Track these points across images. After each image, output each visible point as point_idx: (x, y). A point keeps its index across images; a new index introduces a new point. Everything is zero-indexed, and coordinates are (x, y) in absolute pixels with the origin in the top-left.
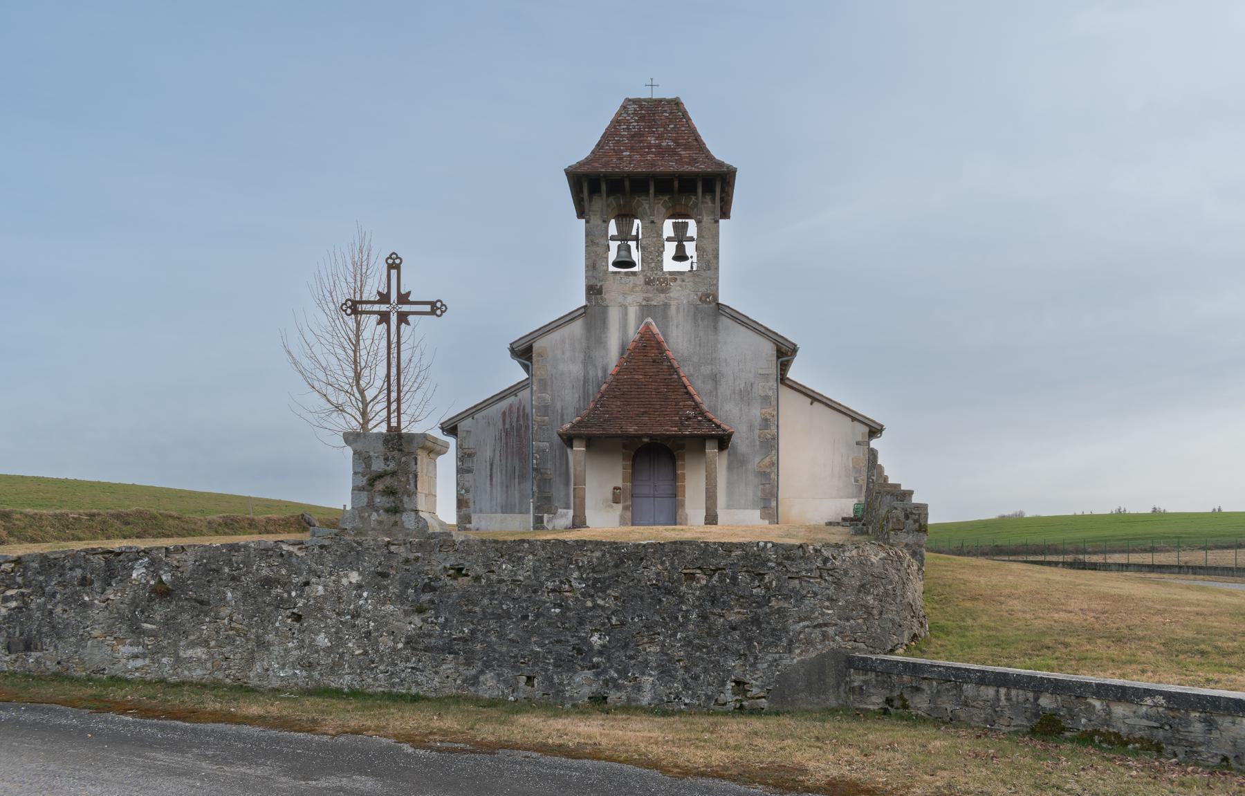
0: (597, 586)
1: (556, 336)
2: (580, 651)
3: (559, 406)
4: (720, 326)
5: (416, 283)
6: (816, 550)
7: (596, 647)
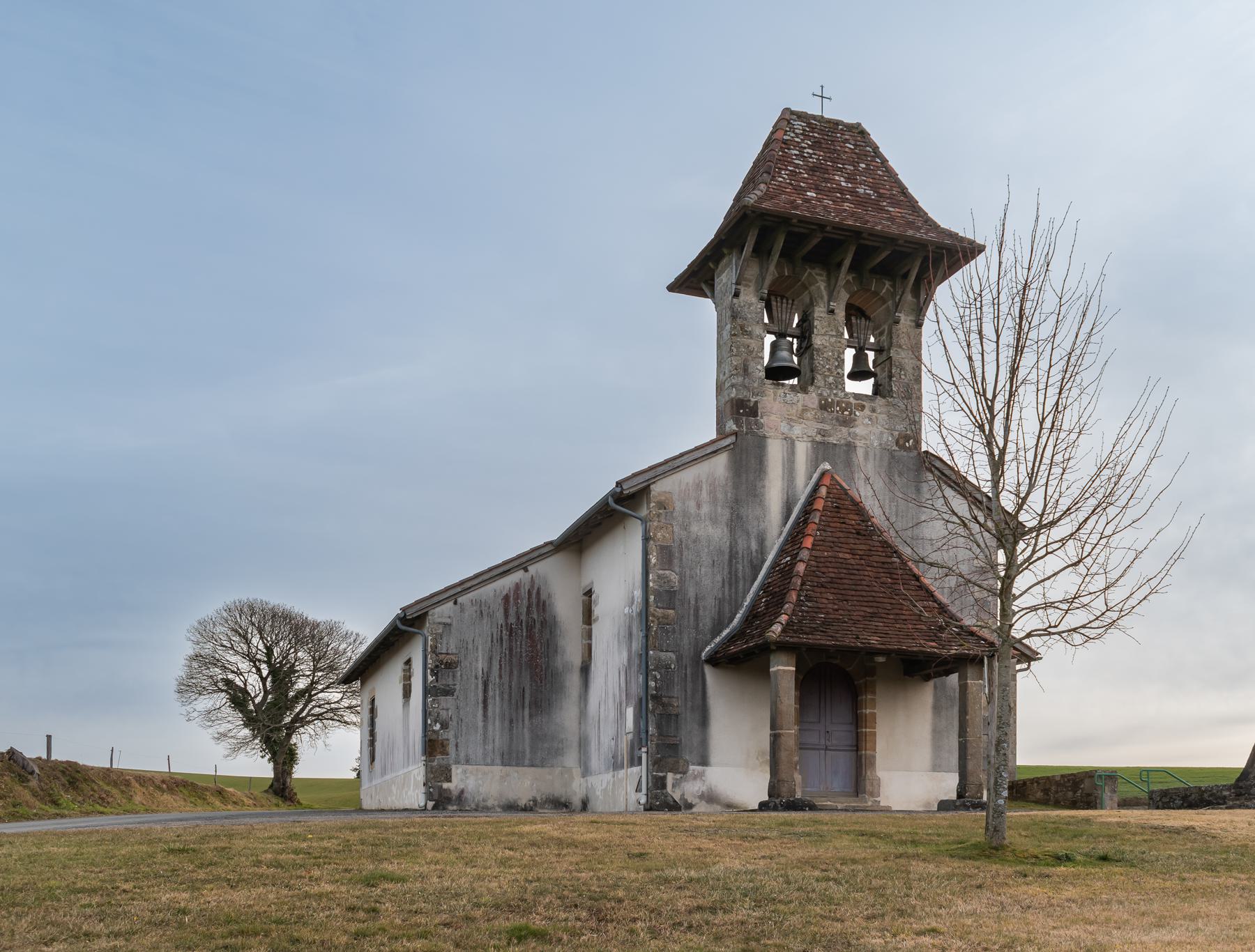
1: (688, 476)
3: (691, 593)
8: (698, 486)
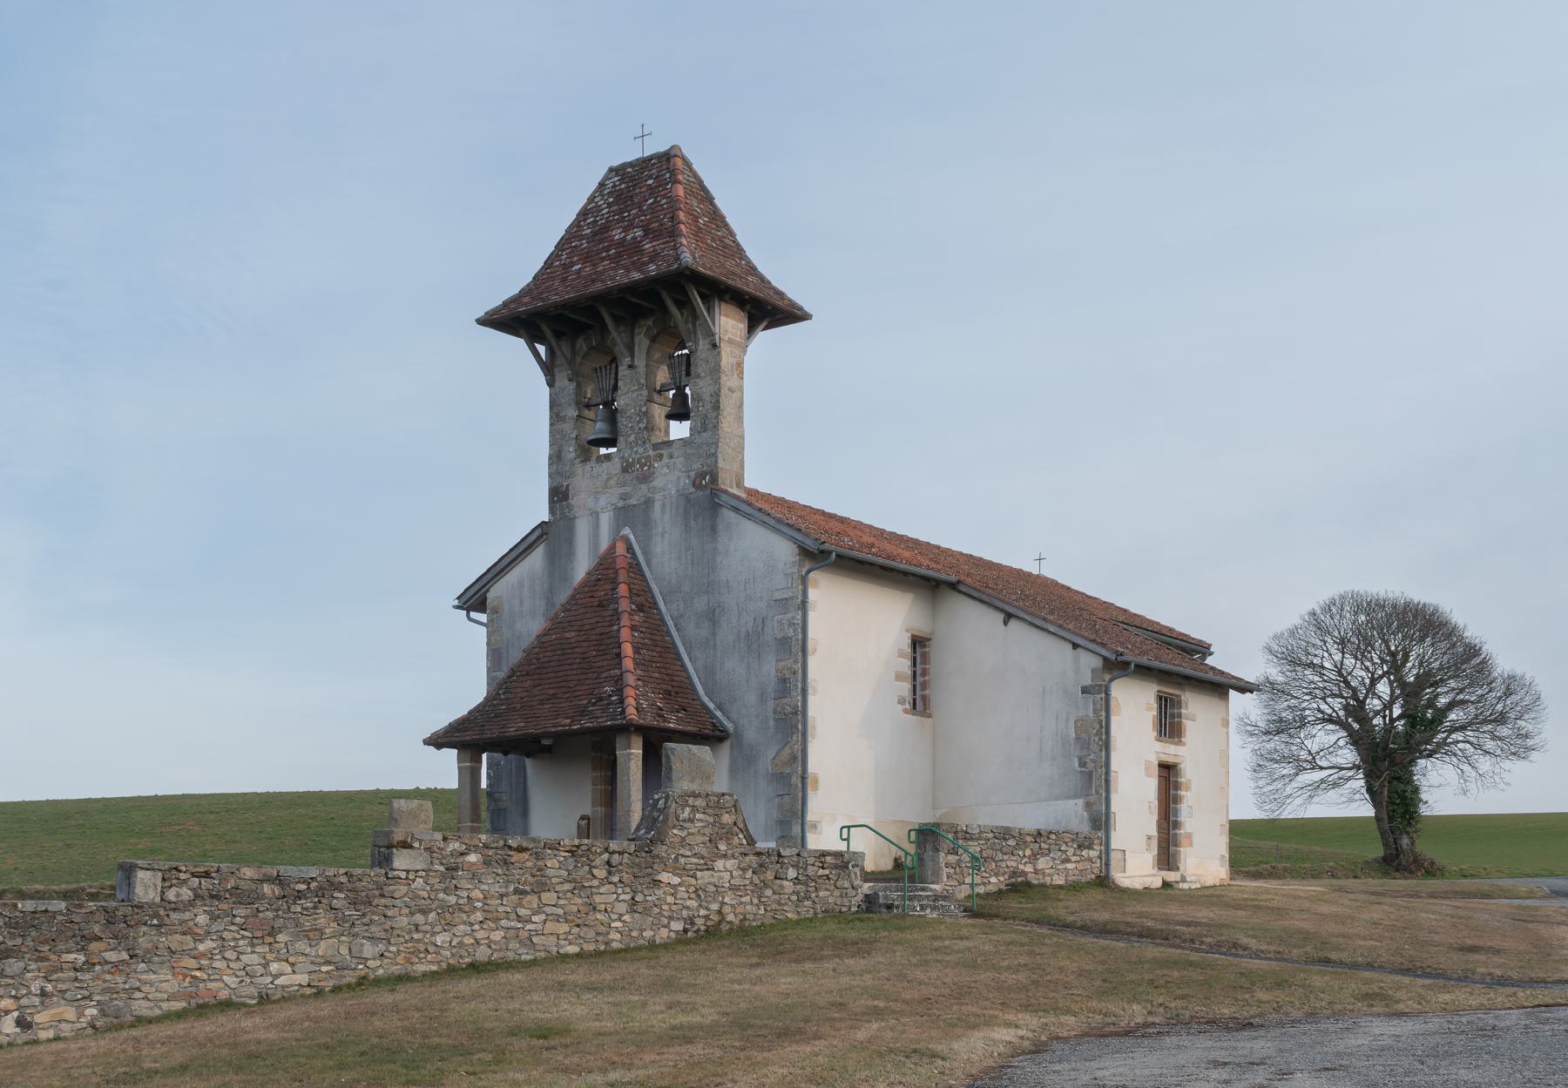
8: (521, 584)
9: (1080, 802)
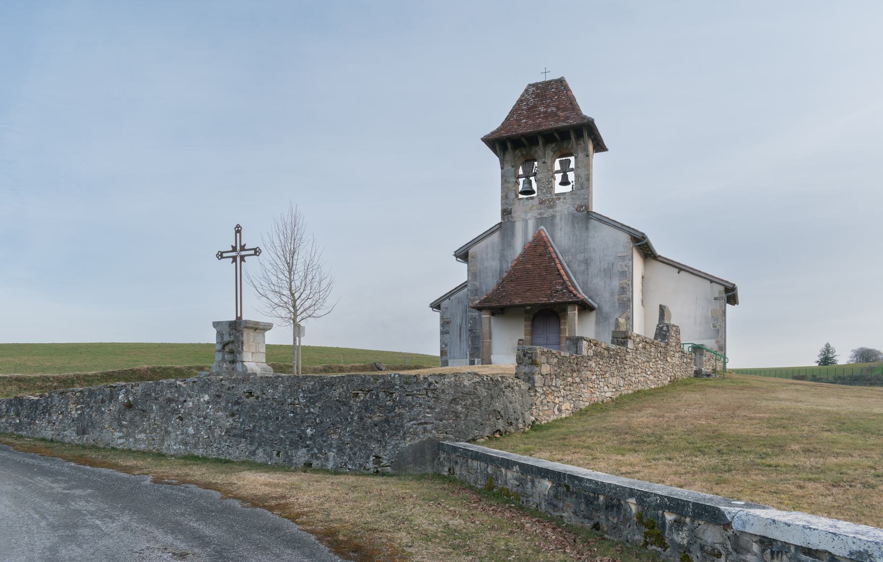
0: (311, 402)
2: (301, 438)
3: (484, 289)
4: (590, 226)
5: (249, 241)
6: (425, 378)
7: (309, 435)
8: (487, 247)
9: (714, 341)
